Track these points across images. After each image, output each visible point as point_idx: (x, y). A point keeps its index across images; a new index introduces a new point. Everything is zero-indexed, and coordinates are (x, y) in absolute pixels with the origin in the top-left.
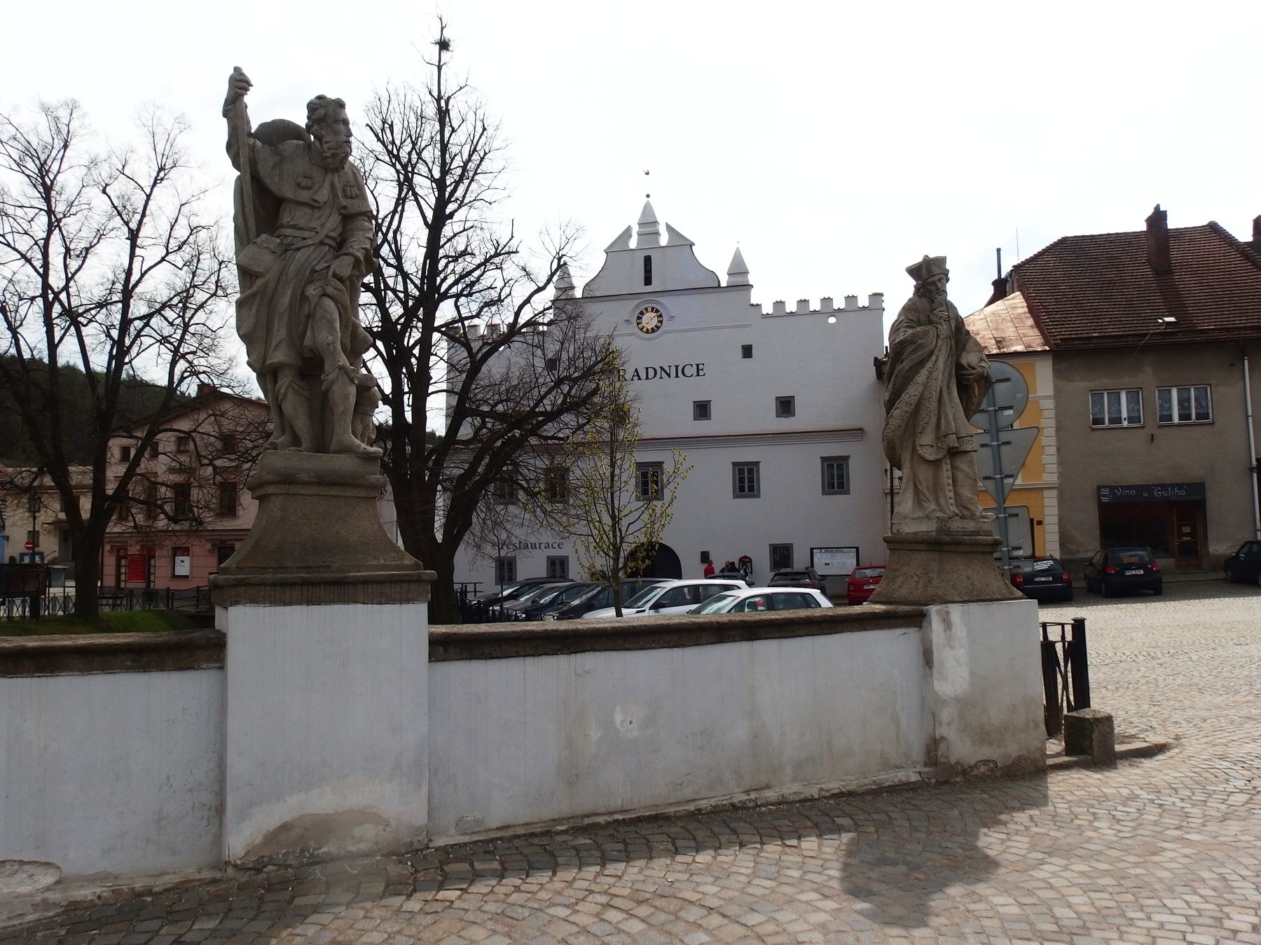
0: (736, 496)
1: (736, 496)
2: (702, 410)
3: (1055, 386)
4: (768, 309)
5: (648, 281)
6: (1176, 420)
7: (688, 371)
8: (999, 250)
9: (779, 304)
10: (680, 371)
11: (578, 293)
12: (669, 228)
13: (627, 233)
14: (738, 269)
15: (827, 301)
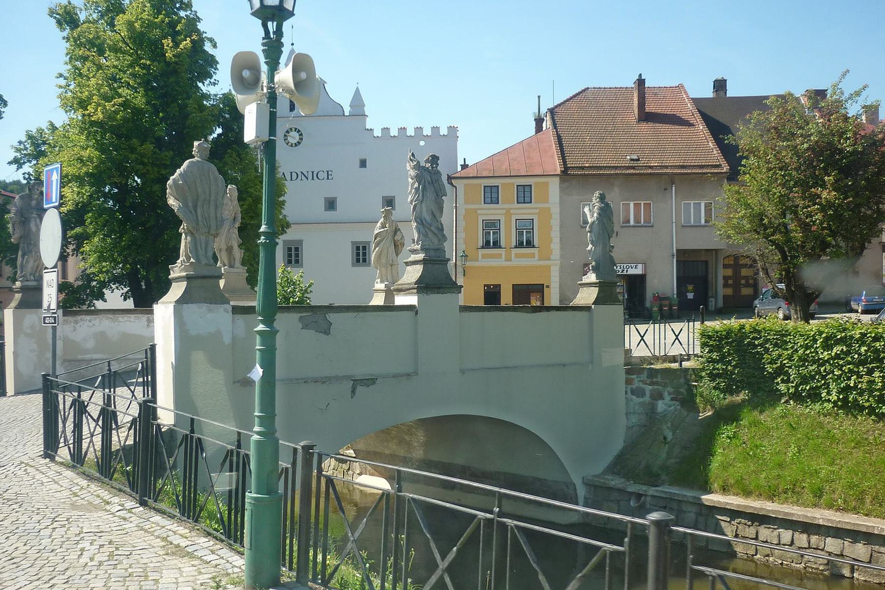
0: (353, 265)
1: (353, 265)
2: (331, 204)
3: (560, 198)
4: (378, 133)
6: (632, 223)
7: (321, 175)
8: (539, 97)
9: (386, 130)
10: (315, 176)
14: (357, 101)
15: (419, 129)
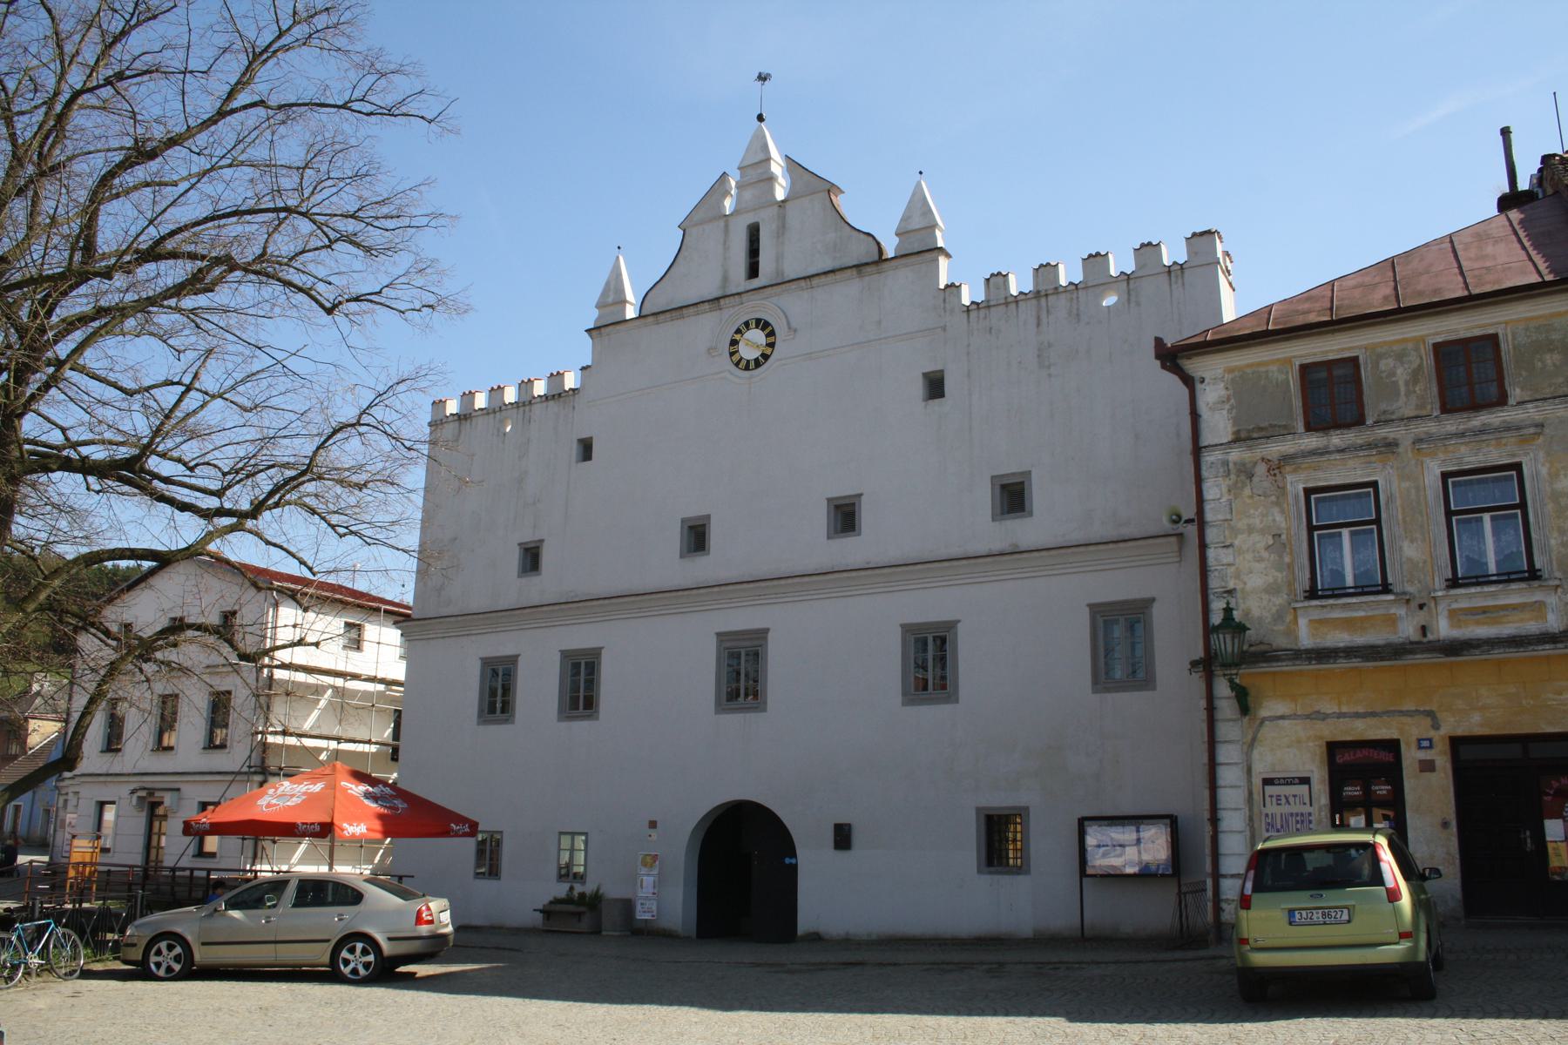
5: (753, 271)
8: (1505, 132)
11: (631, 312)
12: (792, 165)
13: (719, 187)
